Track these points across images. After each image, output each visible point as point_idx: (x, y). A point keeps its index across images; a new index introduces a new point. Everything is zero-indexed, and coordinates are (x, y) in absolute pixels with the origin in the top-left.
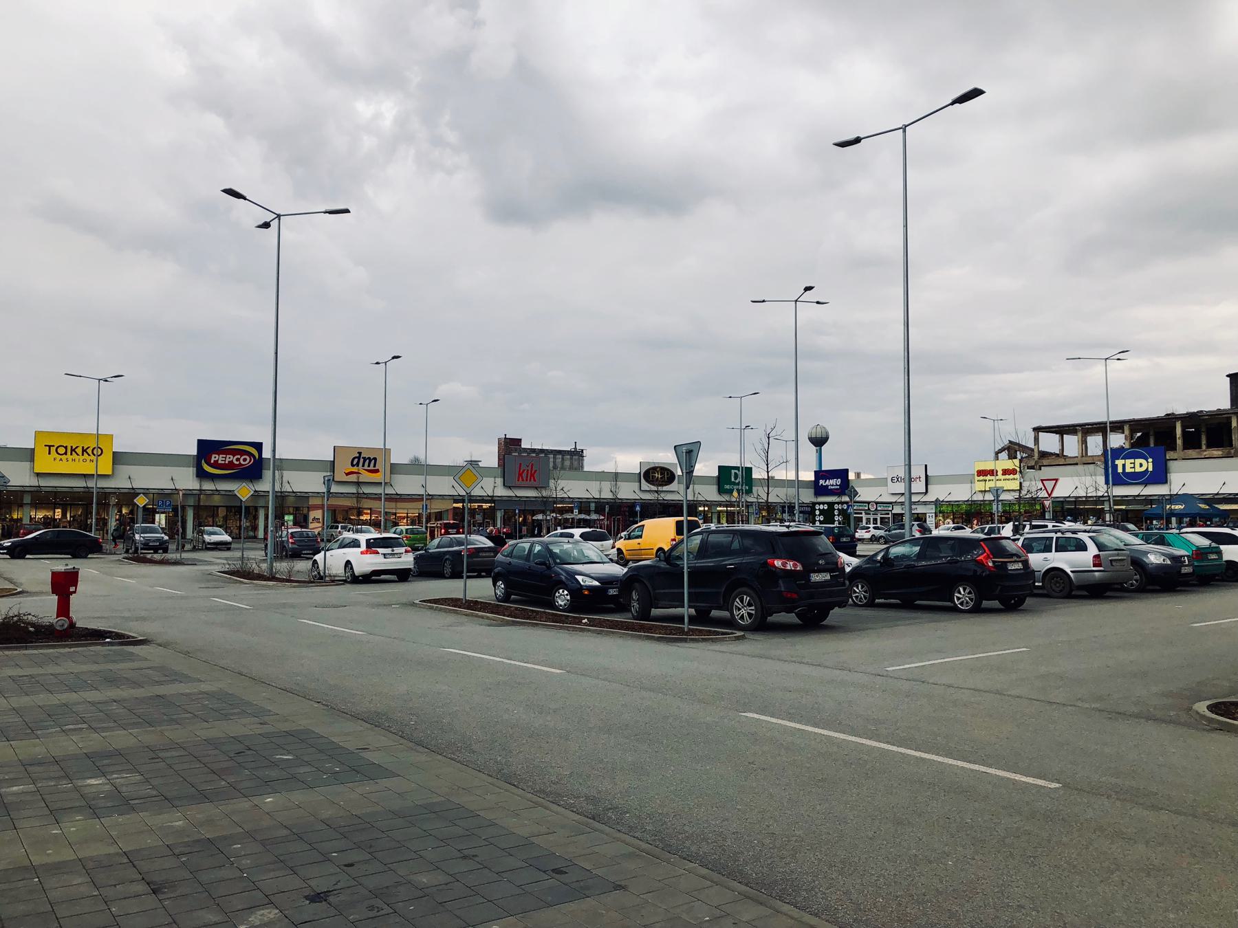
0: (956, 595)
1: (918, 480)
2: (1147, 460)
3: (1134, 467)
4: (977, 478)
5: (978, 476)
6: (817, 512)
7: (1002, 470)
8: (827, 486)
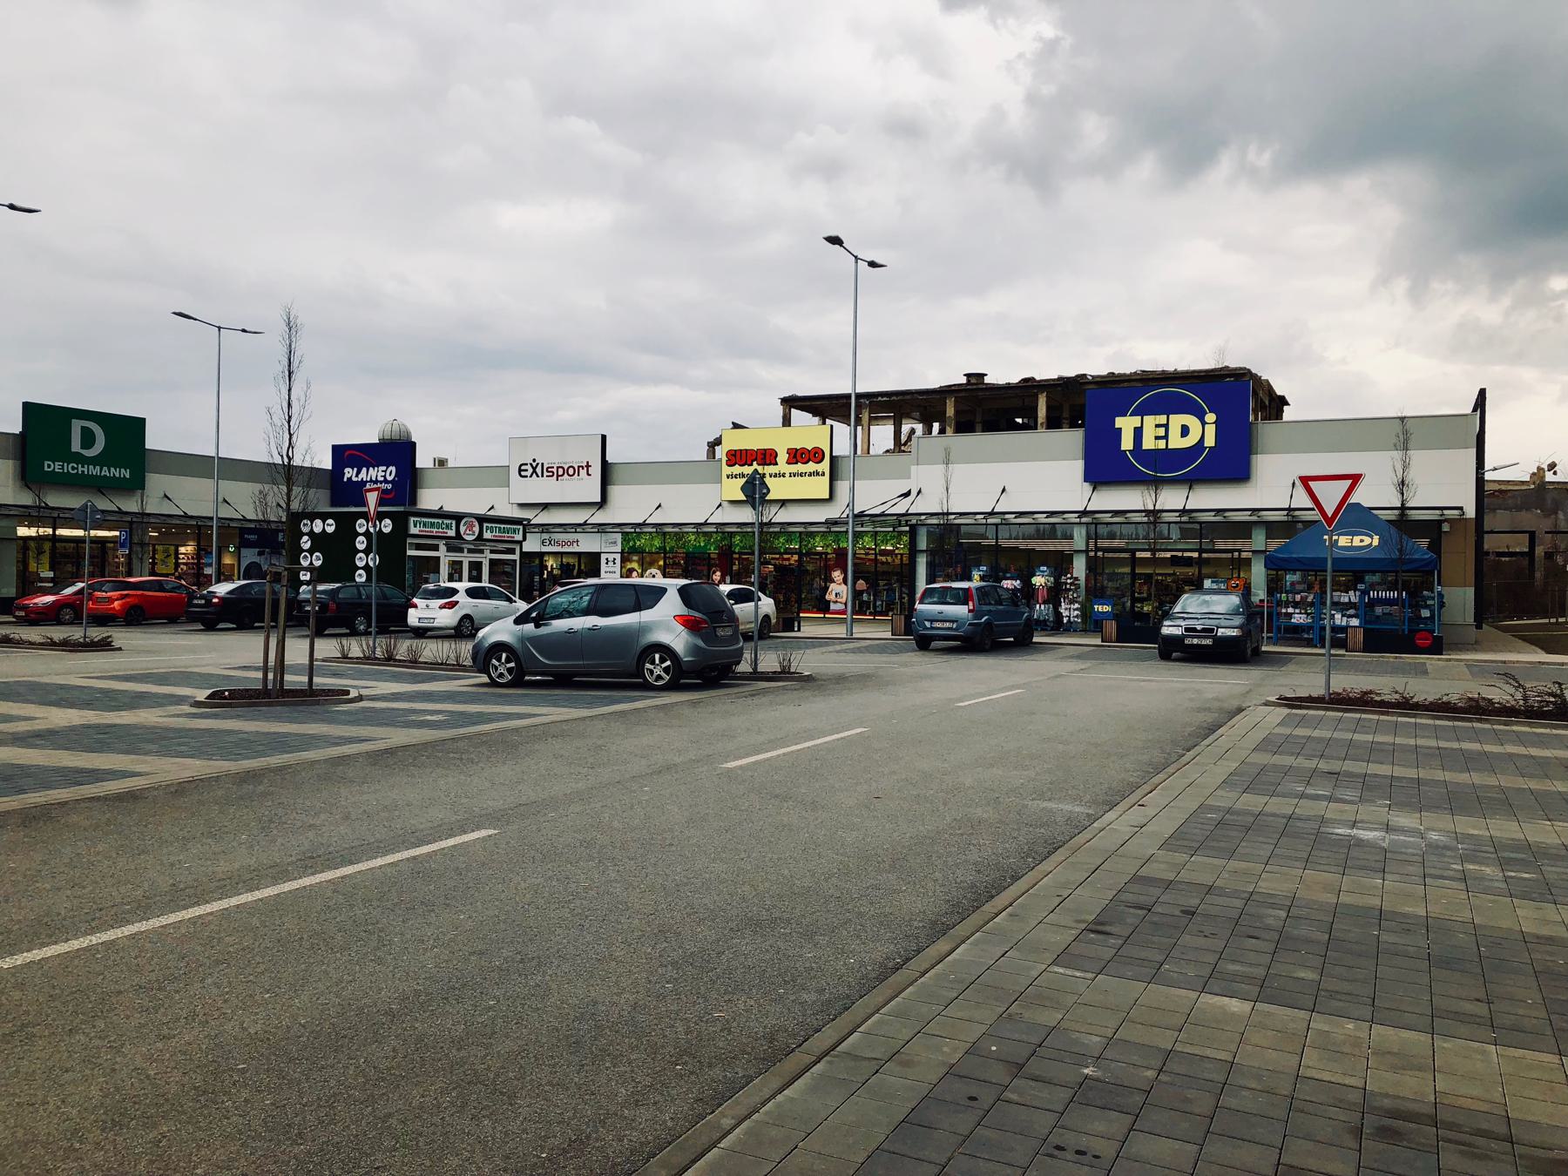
1: (583, 472)
2: (1201, 417)
3: (1166, 437)
4: (727, 470)
5: (729, 465)
6: (306, 543)
7: (789, 451)
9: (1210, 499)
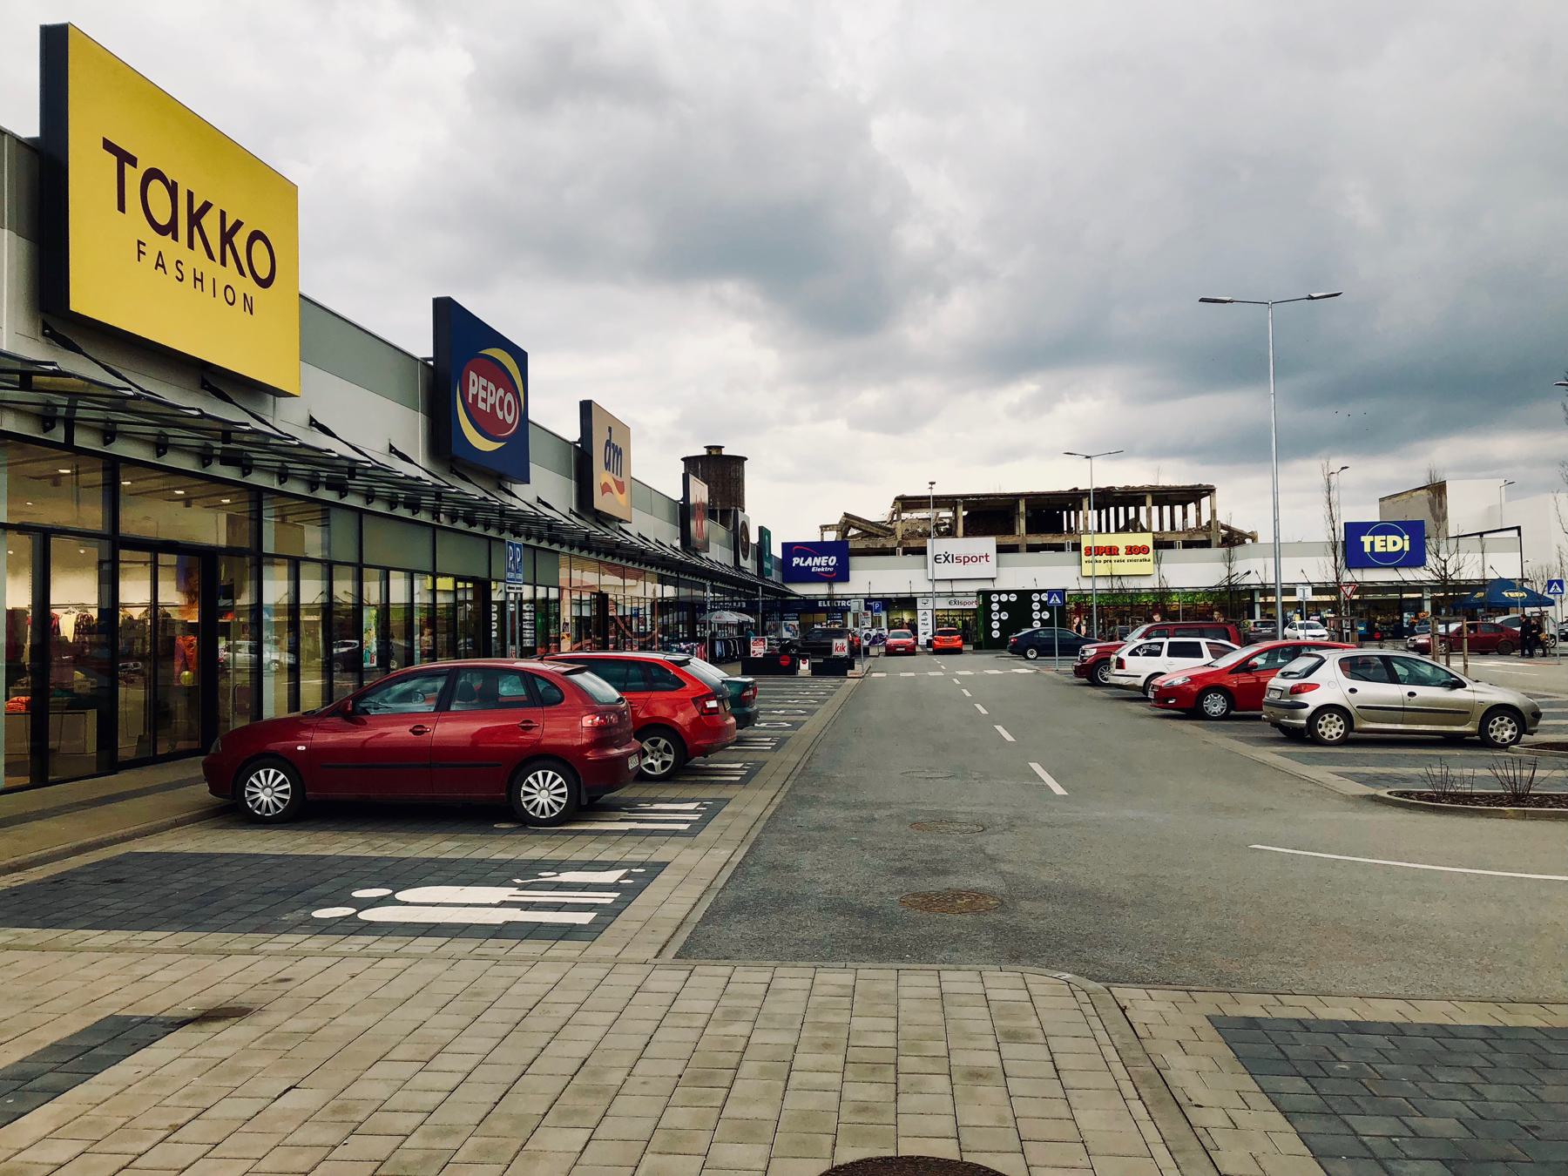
0: (251, 779)
1: (983, 560)
2: (1402, 537)
3: (1386, 546)
6: (995, 607)
7: (1126, 547)
8: (809, 568)
9: (1408, 575)
